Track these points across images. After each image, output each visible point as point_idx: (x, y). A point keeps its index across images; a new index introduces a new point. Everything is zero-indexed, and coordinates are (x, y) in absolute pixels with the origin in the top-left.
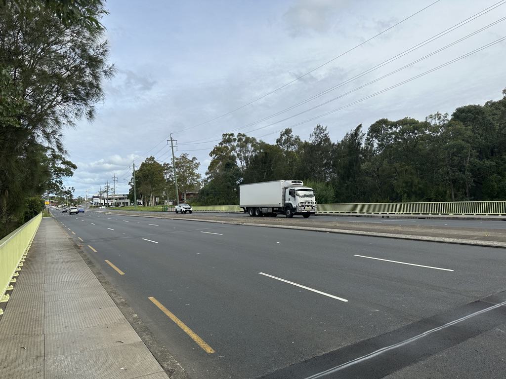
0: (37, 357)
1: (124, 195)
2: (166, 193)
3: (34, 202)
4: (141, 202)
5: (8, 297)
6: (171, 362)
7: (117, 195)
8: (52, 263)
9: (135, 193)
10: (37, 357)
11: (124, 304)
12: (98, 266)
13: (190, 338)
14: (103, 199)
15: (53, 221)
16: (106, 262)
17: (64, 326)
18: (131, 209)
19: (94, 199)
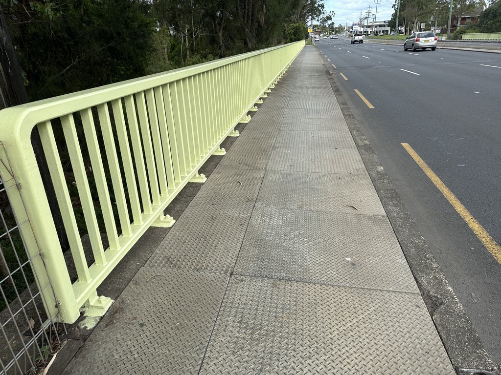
0: (249, 200)
1: (384, 22)
2: (435, 18)
3: (297, 28)
4: (403, 29)
5: (249, 118)
6: (435, 277)
7: (377, 22)
8: (300, 87)
9: (397, 18)
10: (249, 200)
11: (367, 148)
12: (346, 96)
13: (465, 225)
14: (362, 27)
15: (313, 49)
16: (354, 91)
17: (289, 164)
18: (390, 37)
19: (354, 26)
